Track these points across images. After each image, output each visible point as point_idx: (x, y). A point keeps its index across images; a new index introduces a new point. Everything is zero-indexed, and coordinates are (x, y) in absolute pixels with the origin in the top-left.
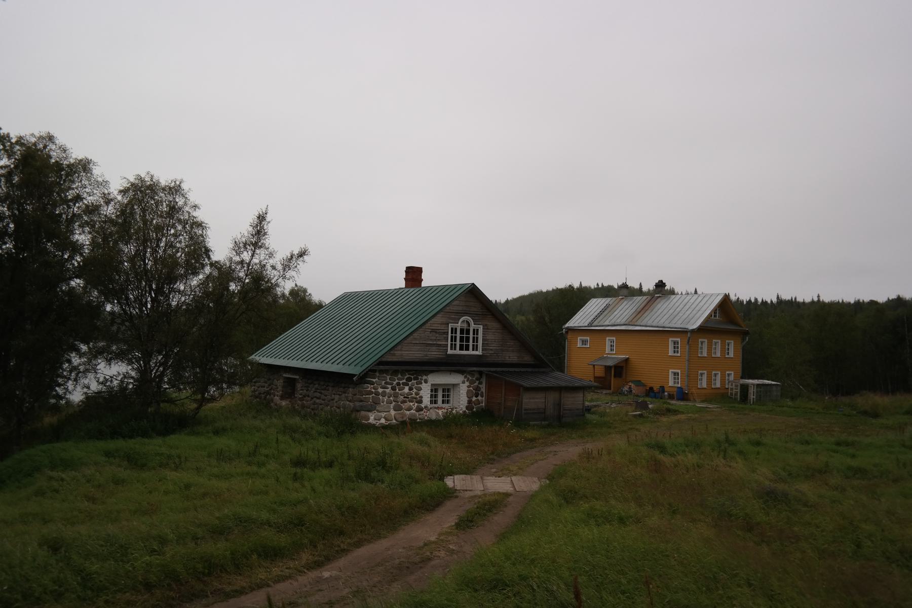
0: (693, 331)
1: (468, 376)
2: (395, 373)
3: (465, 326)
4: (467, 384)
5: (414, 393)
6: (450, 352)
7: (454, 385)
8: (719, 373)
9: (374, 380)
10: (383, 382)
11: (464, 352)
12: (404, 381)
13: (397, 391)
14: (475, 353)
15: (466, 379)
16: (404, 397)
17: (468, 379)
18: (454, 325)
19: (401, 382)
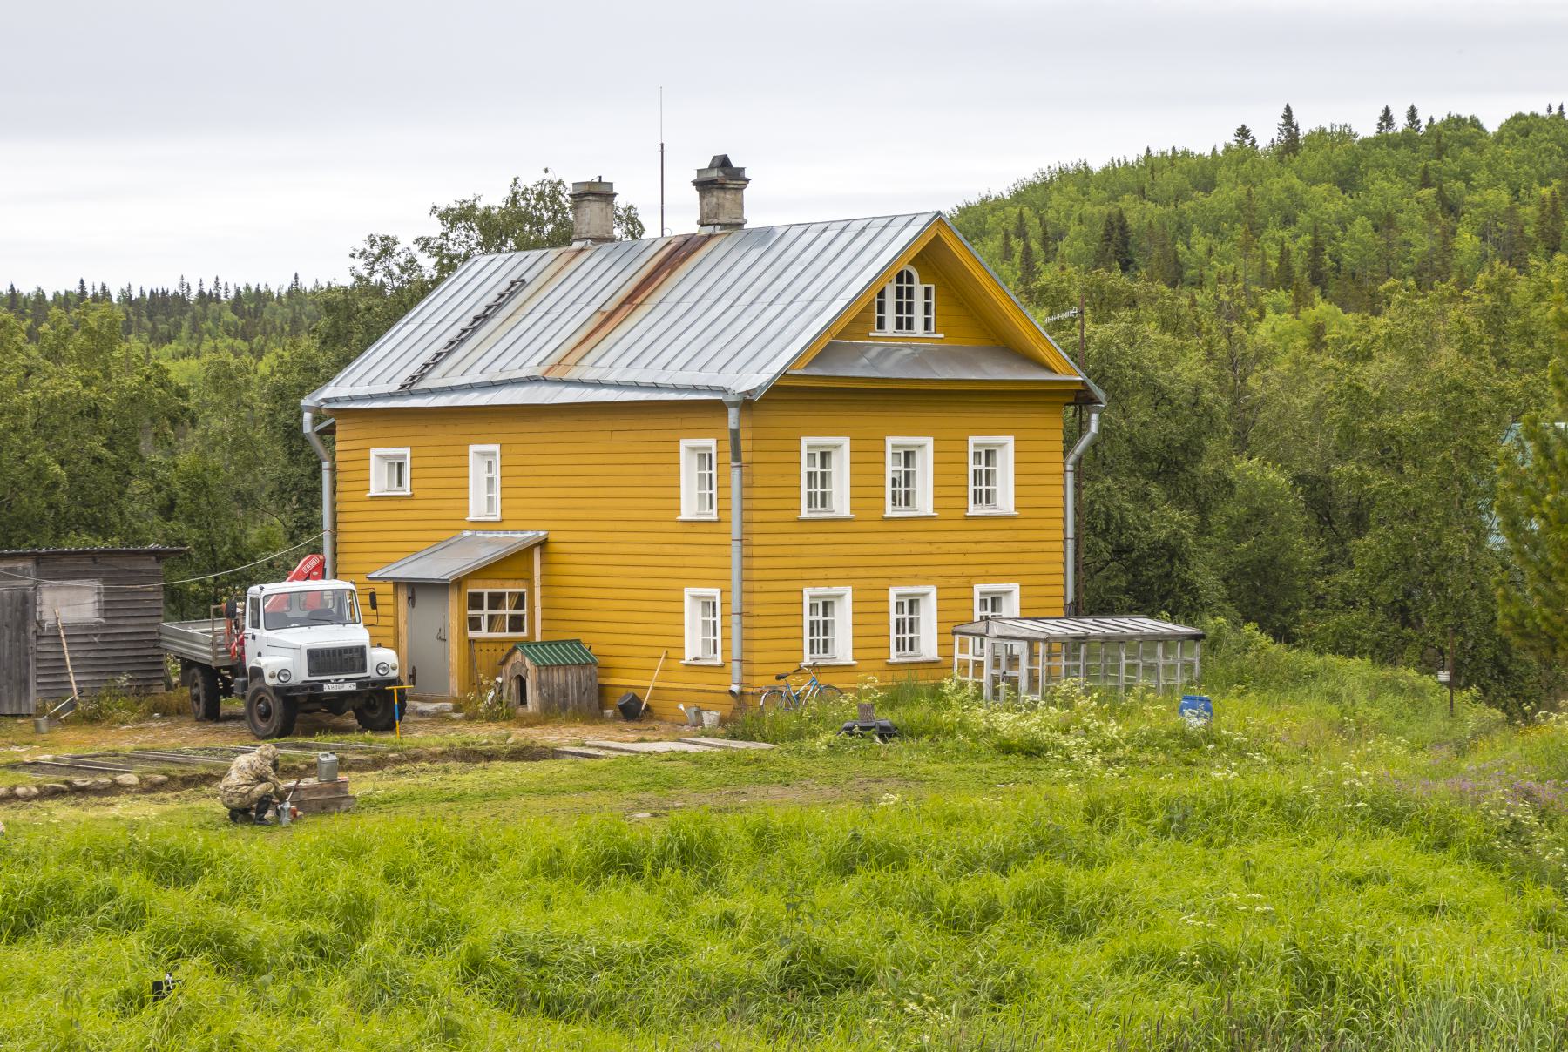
0: (747, 404)
8: (933, 591)
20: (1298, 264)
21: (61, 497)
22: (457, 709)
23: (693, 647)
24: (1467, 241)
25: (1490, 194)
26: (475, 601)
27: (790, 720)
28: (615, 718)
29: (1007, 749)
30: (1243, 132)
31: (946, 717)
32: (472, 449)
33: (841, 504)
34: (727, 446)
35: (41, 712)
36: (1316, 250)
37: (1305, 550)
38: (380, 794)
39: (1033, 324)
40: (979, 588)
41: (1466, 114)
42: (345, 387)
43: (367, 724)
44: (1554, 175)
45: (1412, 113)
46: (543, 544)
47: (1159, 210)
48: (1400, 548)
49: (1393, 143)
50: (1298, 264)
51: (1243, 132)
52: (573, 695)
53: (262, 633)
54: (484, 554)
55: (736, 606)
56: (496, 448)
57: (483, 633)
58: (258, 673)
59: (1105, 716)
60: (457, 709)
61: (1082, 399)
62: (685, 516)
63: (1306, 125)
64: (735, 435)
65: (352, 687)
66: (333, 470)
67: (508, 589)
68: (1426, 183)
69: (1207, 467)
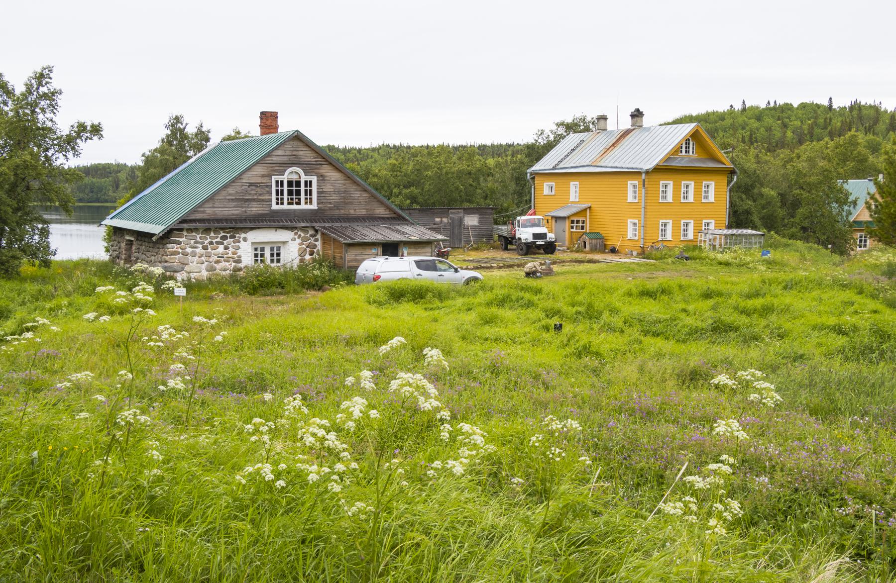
0: (647, 172)
1: (299, 233)
2: (207, 230)
3: (294, 177)
4: (299, 241)
5: (230, 252)
6: (275, 207)
7: (284, 243)
8: (692, 222)
9: (181, 240)
10: (192, 242)
11: (294, 207)
12: (218, 239)
13: (209, 250)
14: (309, 207)
15: (296, 237)
16: (219, 257)
17: (300, 236)
18: (279, 178)
19: (214, 241)
20: (747, 139)
21: (462, 194)
22: (568, 249)
23: (630, 235)
24: (789, 134)
25: (795, 123)
26: (573, 222)
27: (658, 254)
28: (609, 252)
29: (720, 263)
30: (732, 106)
31: (703, 255)
32: (571, 183)
33: (670, 199)
34: (642, 183)
35: (465, 247)
36: (751, 136)
37: (781, 212)
38: (559, 271)
39: (721, 154)
40: (682, 222)
41: (789, 102)
42: (539, 167)
43: (547, 252)
44: (811, 118)
45: (775, 102)
46: (590, 208)
47: (710, 125)
48: (810, 212)
49: (770, 109)
50: (747, 139)
51: (732, 106)
52: (598, 246)
53: (520, 229)
54: (574, 210)
55: (642, 225)
56: (578, 183)
57: (574, 230)
58: (520, 239)
59: (746, 255)
60: (568, 249)
61: (732, 172)
62: (629, 201)
63: (748, 105)
64: (644, 180)
65: (543, 243)
66: (534, 188)
67: (581, 219)
68: (779, 119)
69: (756, 191)
